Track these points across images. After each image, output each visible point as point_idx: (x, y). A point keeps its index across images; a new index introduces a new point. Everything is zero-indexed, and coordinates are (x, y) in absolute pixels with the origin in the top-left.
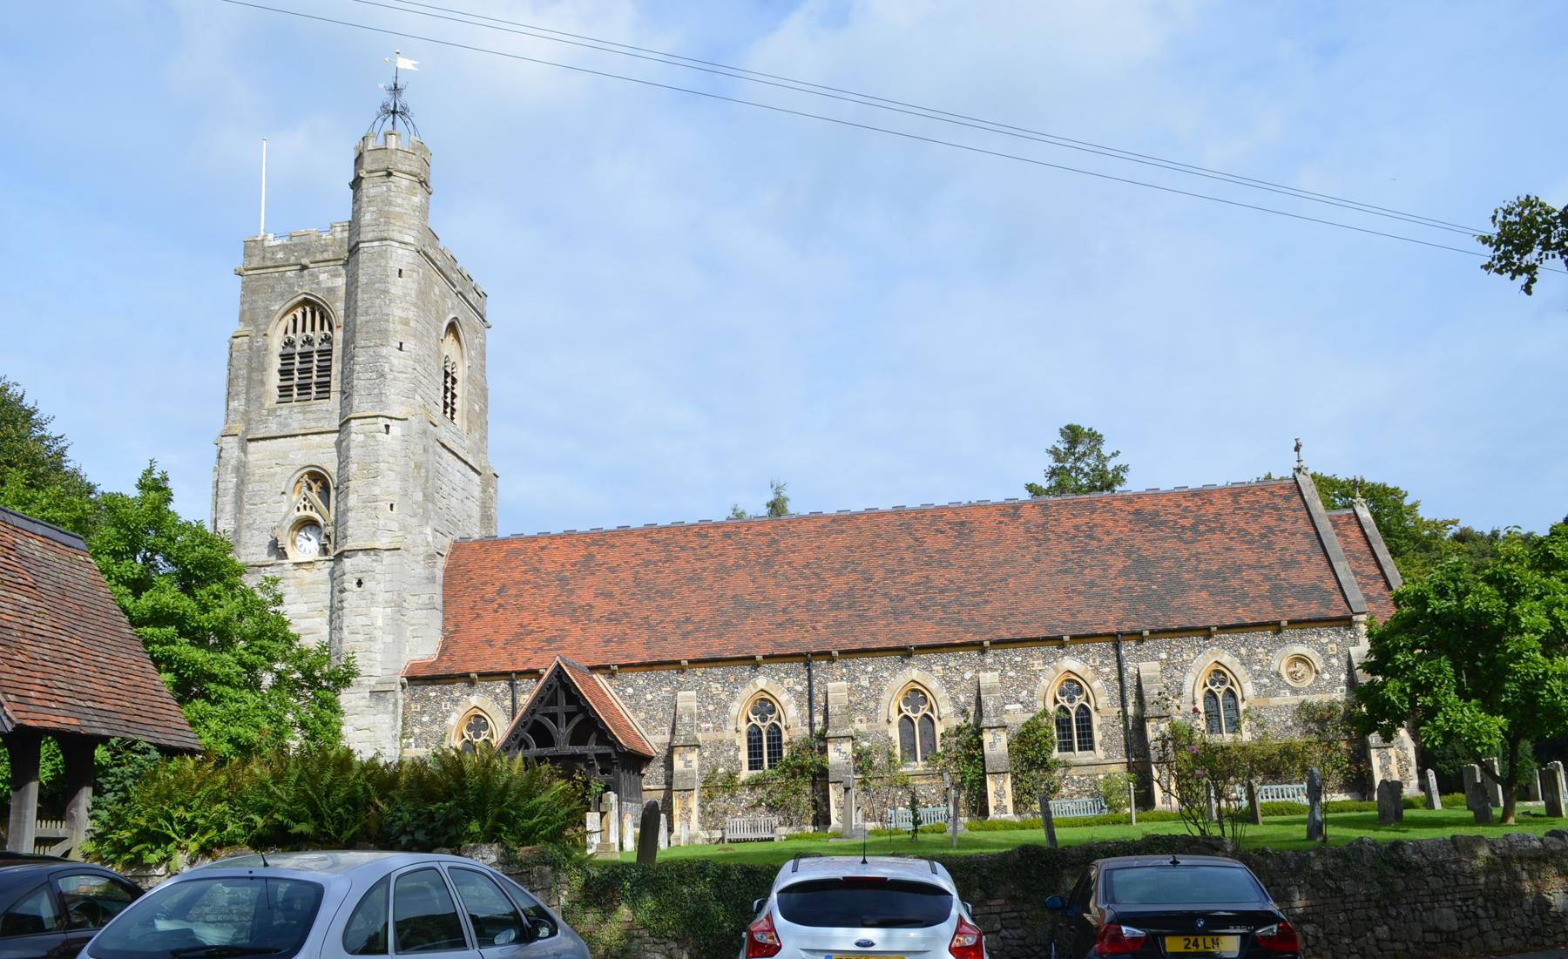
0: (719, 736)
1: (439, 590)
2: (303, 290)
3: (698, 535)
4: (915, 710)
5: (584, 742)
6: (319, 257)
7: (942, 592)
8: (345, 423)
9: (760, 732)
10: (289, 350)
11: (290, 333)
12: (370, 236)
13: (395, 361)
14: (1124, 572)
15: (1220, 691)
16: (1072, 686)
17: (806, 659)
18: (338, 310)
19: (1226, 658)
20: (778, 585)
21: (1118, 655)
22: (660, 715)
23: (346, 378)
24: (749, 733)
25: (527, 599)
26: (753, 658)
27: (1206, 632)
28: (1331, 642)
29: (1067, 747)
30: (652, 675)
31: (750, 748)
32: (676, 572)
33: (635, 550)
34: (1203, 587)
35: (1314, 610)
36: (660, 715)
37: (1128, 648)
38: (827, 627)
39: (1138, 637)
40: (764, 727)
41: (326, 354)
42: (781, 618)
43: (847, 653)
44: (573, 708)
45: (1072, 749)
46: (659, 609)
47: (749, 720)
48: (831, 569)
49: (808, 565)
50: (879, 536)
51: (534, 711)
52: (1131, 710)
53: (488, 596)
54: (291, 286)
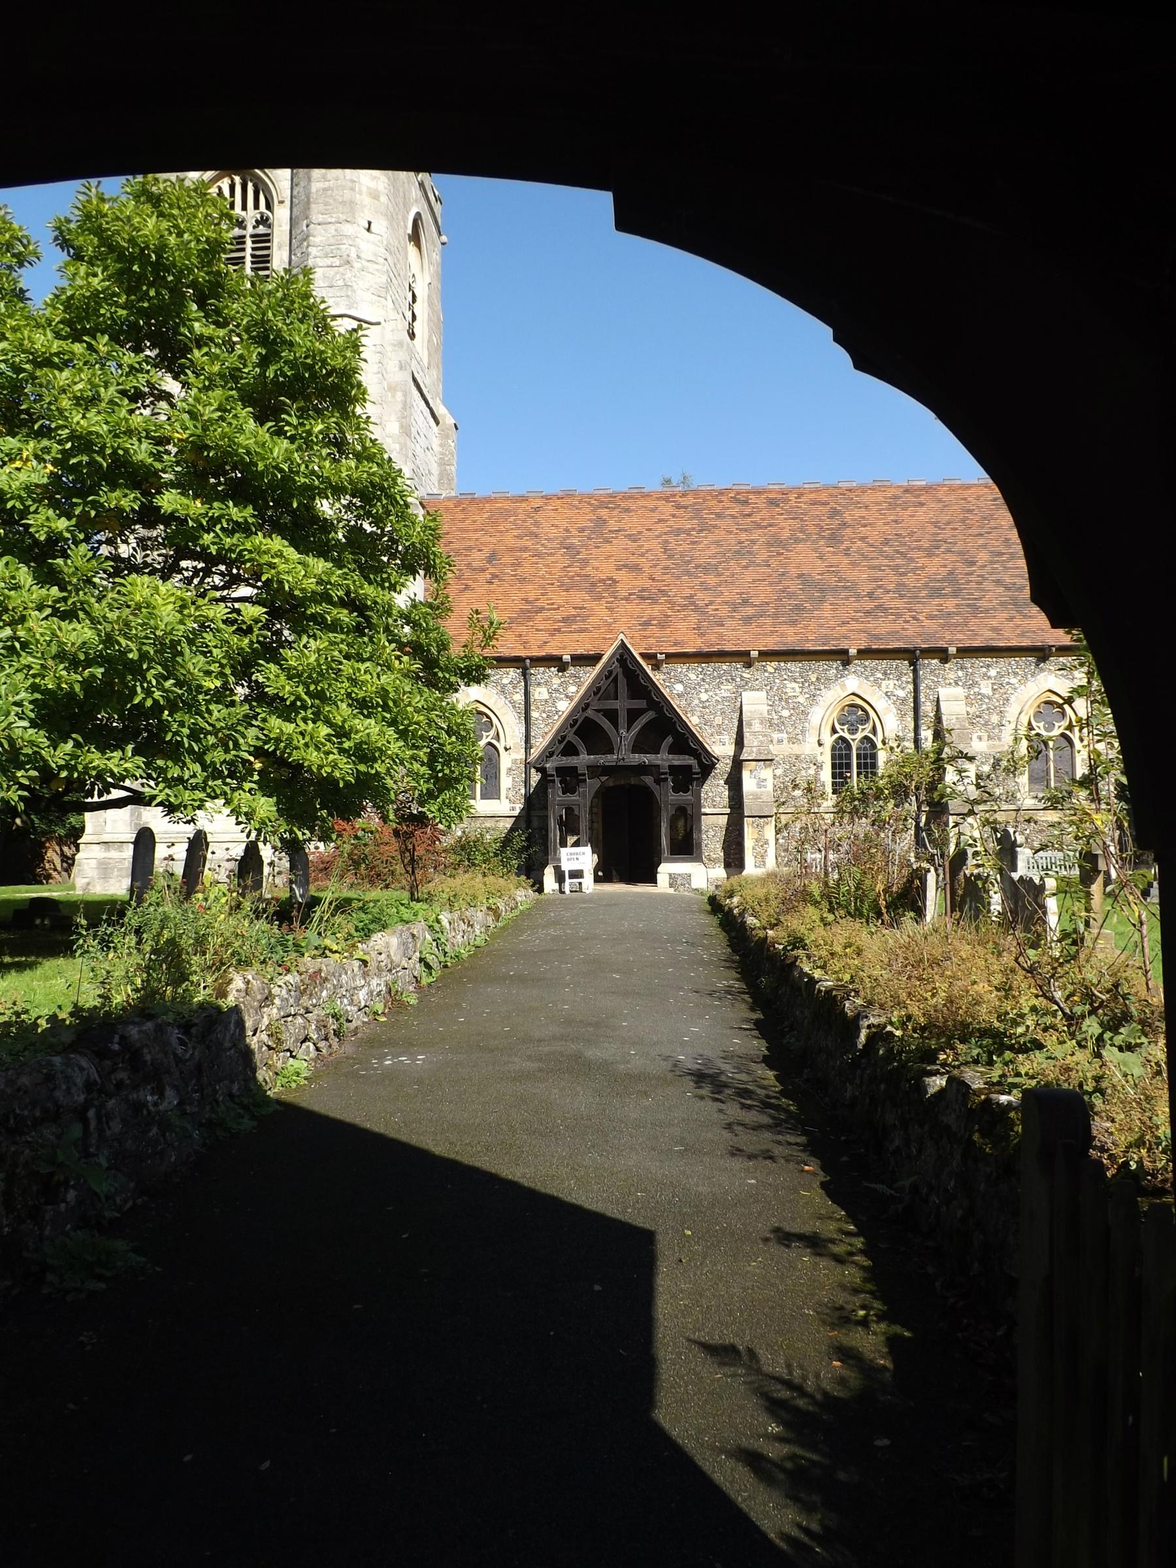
0: (796, 749)
3: (735, 500)
4: (852, 731)
9: (849, 747)
13: (364, 246)
17: (912, 656)
20: (853, 564)
22: (718, 720)
24: (833, 748)
25: (526, 569)
26: (846, 652)
30: (709, 668)
31: (834, 766)
32: (717, 543)
36: (718, 720)
38: (930, 617)
40: (855, 739)
42: (871, 605)
43: (966, 652)
44: (641, 704)
46: (705, 587)
47: (834, 731)
48: (919, 548)
49: (886, 542)
50: (970, 511)
51: (587, 705)
53: (475, 564)
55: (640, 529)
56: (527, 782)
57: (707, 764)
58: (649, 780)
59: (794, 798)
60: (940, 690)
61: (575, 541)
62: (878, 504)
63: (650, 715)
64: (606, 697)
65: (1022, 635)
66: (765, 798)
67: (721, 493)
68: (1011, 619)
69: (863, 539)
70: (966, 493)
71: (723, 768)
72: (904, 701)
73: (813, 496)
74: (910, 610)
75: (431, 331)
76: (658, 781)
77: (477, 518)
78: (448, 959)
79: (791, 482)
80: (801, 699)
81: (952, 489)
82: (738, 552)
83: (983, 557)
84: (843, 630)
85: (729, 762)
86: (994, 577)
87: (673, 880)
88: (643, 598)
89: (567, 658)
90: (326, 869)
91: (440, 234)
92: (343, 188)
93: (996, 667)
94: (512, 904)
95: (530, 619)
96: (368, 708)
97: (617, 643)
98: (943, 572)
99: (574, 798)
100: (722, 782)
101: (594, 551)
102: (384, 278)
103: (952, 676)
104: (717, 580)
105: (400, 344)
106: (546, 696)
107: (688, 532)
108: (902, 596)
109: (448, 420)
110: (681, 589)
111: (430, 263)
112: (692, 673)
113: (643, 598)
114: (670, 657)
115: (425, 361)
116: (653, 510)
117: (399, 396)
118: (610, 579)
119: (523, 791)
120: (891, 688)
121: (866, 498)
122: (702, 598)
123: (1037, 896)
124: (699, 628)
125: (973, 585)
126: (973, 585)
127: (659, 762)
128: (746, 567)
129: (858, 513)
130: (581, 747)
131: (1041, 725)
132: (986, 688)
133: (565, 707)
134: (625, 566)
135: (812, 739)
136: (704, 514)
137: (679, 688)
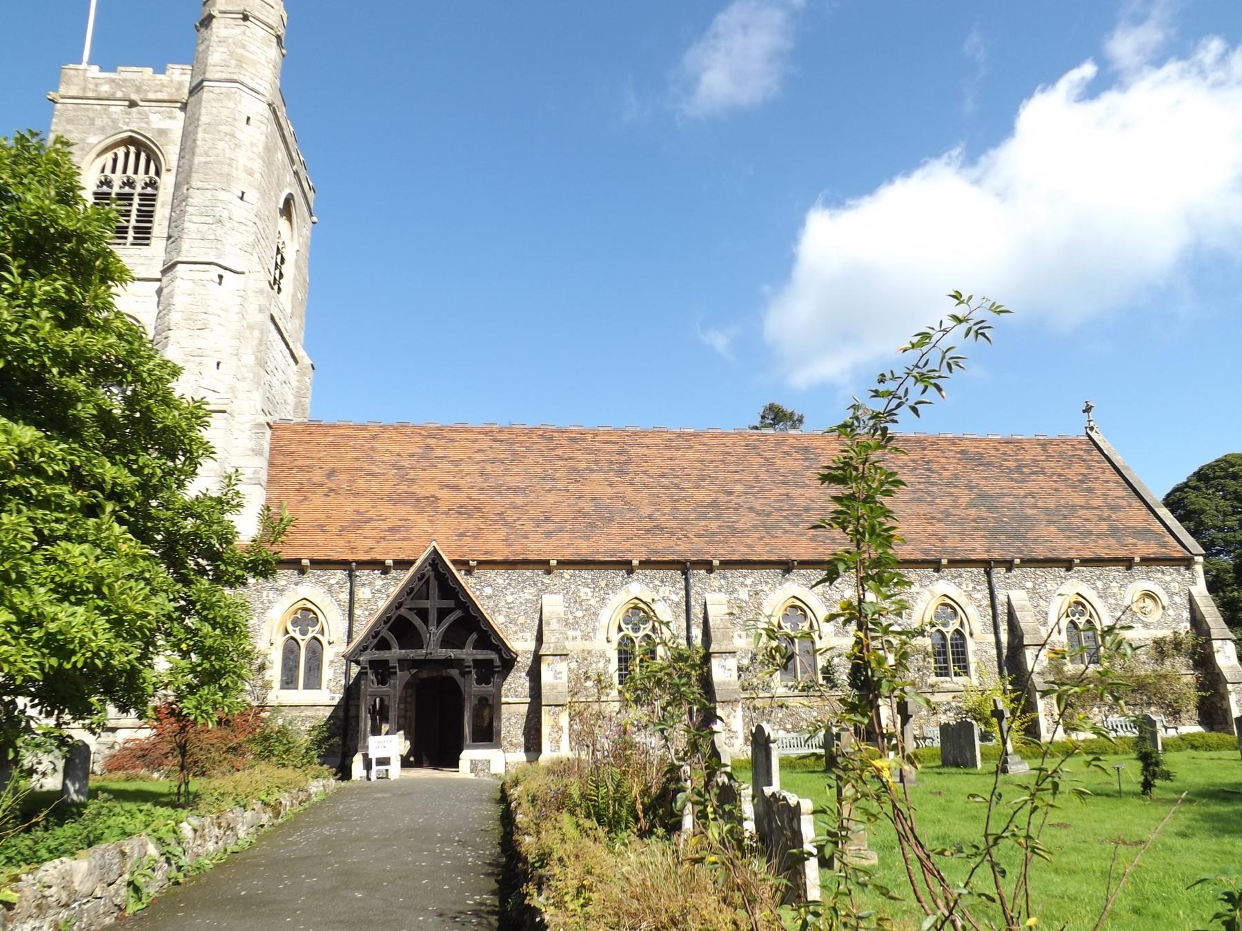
0: (588, 645)
1: (265, 465)
2: (131, 123)
3: (542, 437)
4: (636, 630)
5: (461, 647)
6: (152, 96)
7: (807, 509)
8: (169, 268)
10: (105, 189)
11: (108, 172)
12: (218, 76)
14: (972, 504)
15: (1082, 622)
16: (950, 608)
17: (683, 567)
18: (170, 155)
19: (954, 592)
20: (637, 491)
21: (990, 582)
22: (522, 619)
23: (175, 222)
24: (620, 644)
25: (360, 485)
26: (630, 562)
27: (1068, 564)
28: (1173, 580)
29: (943, 672)
30: (515, 574)
33: (477, 447)
34: (1050, 523)
35: (1153, 550)
36: (522, 619)
37: (999, 573)
38: (699, 536)
39: (1009, 565)
41: (149, 200)
42: (649, 525)
43: (727, 564)
44: (450, 603)
45: (947, 675)
46: (514, 506)
47: (620, 629)
48: (689, 481)
49: (663, 475)
52: (1004, 637)
54: (115, 121)
55: (462, 456)
56: (347, 673)
57: (508, 662)
58: (454, 673)
59: (586, 689)
60: (707, 595)
61: (406, 464)
62: (656, 445)
63: (457, 614)
64: (419, 596)
65: (771, 551)
66: (560, 689)
67: (531, 431)
68: (761, 538)
69: (644, 472)
70: (726, 439)
71: (524, 661)
72: (678, 605)
73: (605, 437)
74: (682, 529)
75: (296, 288)
76: (463, 674)
77: (321, 441)
78: (181, 875)
79: (587, 425)
80: (593, 602)
81: (714, 436)
82: (543, 479)
83: (739, 489)
84: (628, 544)
85: (531, 656)
86: (747, 505)
87: (474, 766)
88: (460, 513)
89: (389, 562)
90: (144, 756)
91: (311, 215)
92: (222, 163)
93: (751, 577)
94: (302, 796)
95: (359, 528)
96: (76, 593)
97: (430, 549)
98: (708, 499)
99: (385, 689)
100: (524, 674)
101: (421, 473)
102: (252, 238)
103: (716, 584)
104: (525, 500)
105: (261, 292)
106: (369, 595)
107: (502, 461)
108: (675, 518)
109: (306, 360)
110: (493, 508)
111: (300, 235)
112: (500, 578)
113: (460, 513)
114: (481, 563)
115: (289, 311)
116: (474, 442)
117: (257, 334)
118: (433, 496)
119: (343, 682)
120: (667, 594)
121: (647, 440)
122: (511, 515)
123: (791, 820)
124: (507, 540)
125: (731, 511)
126: (731, 511)
127: (464, 657)
128: (549, 491)
129: (641, 451)
130: (394, 642)
131: (788, 625)
132: (743, 594)
133: (382, 604)
134: (447, 486)
135: (601, 636)
136: (516, 447)
137: (488, 590)
